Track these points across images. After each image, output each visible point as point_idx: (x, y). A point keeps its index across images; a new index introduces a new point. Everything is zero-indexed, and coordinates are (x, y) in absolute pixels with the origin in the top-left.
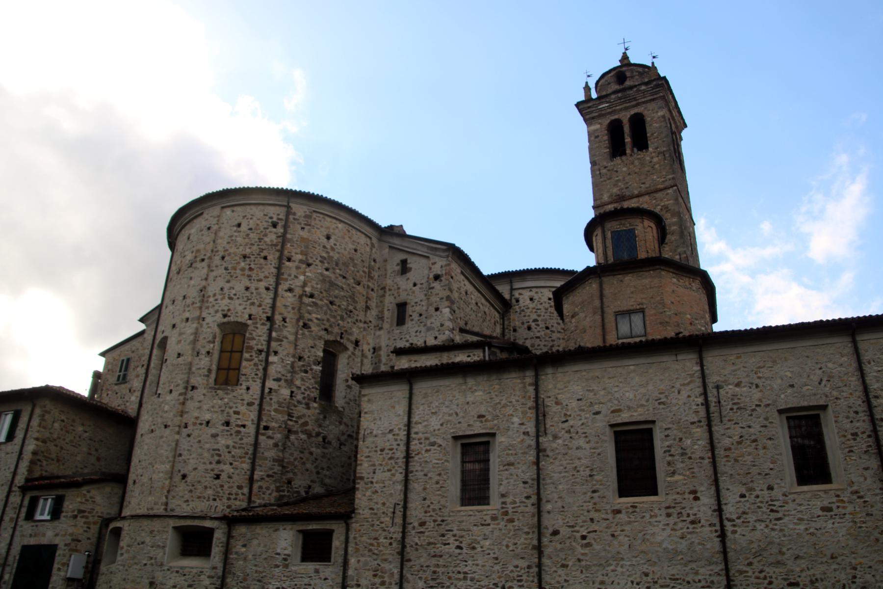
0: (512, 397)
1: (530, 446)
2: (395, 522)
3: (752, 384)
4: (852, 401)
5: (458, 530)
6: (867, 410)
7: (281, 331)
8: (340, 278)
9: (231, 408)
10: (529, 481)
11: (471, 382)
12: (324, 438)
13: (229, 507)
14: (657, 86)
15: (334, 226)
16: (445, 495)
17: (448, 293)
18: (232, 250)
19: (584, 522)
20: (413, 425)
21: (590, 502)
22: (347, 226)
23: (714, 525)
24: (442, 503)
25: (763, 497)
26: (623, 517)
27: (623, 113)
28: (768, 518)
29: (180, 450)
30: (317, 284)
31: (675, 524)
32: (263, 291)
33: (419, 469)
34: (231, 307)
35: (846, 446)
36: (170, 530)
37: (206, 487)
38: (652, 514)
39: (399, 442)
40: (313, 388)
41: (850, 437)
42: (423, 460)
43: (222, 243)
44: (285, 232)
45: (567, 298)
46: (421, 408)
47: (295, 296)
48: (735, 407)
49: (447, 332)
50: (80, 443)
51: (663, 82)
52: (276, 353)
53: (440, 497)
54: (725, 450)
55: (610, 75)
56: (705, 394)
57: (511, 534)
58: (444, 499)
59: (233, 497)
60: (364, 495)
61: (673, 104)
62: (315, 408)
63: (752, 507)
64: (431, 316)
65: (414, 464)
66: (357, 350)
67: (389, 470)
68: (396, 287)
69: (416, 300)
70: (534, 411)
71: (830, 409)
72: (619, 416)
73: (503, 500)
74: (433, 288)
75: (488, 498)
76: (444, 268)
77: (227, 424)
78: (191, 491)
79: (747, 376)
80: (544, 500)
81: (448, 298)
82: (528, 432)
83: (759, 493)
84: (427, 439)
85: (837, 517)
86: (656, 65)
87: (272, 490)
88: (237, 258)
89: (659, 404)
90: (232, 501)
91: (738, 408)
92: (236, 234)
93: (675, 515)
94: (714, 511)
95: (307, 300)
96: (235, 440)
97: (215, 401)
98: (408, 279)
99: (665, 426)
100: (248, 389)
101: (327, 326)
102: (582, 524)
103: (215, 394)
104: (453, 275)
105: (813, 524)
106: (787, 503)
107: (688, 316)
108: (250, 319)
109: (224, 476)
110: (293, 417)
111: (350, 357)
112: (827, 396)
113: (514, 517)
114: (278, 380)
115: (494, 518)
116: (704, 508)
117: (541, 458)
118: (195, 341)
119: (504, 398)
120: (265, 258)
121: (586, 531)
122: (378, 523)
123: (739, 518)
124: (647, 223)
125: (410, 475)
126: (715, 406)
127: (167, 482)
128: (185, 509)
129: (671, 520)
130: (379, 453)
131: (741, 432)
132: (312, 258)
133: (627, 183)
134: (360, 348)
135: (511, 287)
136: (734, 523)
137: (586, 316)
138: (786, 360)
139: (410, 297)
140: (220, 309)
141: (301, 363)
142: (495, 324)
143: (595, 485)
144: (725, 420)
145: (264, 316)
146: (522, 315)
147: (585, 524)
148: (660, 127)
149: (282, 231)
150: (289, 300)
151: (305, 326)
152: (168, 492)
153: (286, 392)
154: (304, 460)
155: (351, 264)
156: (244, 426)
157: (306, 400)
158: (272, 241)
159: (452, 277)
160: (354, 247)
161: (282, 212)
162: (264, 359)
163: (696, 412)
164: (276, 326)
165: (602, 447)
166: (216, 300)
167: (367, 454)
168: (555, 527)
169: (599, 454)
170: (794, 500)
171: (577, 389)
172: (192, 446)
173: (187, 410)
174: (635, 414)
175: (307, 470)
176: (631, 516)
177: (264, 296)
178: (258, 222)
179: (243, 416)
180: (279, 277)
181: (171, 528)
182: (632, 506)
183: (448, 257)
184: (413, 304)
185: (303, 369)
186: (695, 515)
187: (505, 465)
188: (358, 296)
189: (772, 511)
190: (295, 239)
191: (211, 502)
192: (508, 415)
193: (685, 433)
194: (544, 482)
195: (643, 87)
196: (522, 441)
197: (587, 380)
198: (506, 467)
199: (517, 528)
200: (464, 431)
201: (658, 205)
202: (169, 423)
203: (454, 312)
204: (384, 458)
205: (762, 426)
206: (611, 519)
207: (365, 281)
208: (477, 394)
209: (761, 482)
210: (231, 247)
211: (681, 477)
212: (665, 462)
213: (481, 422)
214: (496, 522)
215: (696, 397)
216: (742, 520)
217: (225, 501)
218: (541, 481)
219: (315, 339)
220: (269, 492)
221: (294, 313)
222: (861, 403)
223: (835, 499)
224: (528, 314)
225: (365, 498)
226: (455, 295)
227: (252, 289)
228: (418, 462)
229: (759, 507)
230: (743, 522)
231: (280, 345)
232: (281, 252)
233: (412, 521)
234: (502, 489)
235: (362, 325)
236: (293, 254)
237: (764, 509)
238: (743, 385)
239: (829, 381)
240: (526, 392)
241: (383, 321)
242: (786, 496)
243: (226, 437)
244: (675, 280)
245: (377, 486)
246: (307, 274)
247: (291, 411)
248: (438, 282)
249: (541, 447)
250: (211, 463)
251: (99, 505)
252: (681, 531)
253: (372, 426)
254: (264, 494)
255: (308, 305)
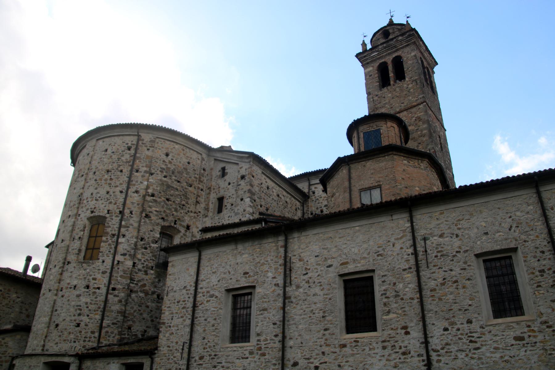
0: (268, 257)
1: (279, 295)
2: (183, 356)
3: (453, 234)
4: (538, 242)
5: (226, 362)
6: (552, 249)
7: (129, 220)
8: (175, 182)
9: (91, 276)
10: (278, 323)
11: (240, 247)
12: (158, 296)
13: (84, 347)
14: (410, 36)
15: (172, 147)
16: (218, 335)
17: (251, 188)
18: (100, 168)
19: (317, 355)
20: (199, 282)
21: (322, 338)
22: (182, 146)
23: (422, 356)
24: (216, 341)
25: (463, 330)
26: (347, 350)
27: (388, 57)
28: (468, 348)
29: (56, 307)
30: (157, 187)
31: (389, 355)
32: (118, 193)
33: (202, 315)
34: (97, 206)
35: (534, 282)
36: (41, 365)
37: (70, 333)
38: (371, 347)
39: (190, 295)
40: (151, 260)
41: (538, 273)
42: (204, 308)
43: (95, 163)
44: (136, 153)
45: (329, 183)
46: (206, 269)
47: (140, 196)
48: (439, 254)
49: (247, 215)
50: (14, 306)
51: (414, 32)
52: (124, 236)
53: (214, 337)
54: (431, 291)
55: (379, 33)
56: (414, 245)
57: (263, 365)
58: (217, 338)
59: (87, 339)
60: (165, 336)
61: (424, 48)
62: (152, 274)
63: (454, 339)
64: (238, 205)
65: (199, 311)
66: (188, 232)
67: (182, 317)
68: (217, 186)
69: (230, 195)
70: (283, 267)
71: (519, 251)
72: (347, 267)
73: (258, 338)
74: (240, 185)
75: (249, 337)
76: (247, 170)
77: (88, 287)
78: (60, 336)
79: (449, 228)
80: (288, 338)
81: (250, 191)
82: (278, 284)
83: (460, 326)
84: (208, 292)
85: (529, 345)
86: (409, 22)
87: (116, 334)
88: (103, 172)
89: (378, 256)
90: (87, 342)
91: (441, 256)
92: (104, 156)
93: (390, 348)
94: (422, 343)
95: (149, 198)
96: (91, 299)
97: (81, 272)
98: (225, 180)
99: (382, 274)
100: (103, 262)
101: (164, 215)
102: (315, 357)
103: (81, 266)
104: (254, 174)
105: (507, 352)
106: (484, 334)
107: (417, 189)
108: (108, 213)
109: (82, 324)
110: (134, 281)
111: (182, 237)
112: (516, 240)
113: (266, 352)
114: (124, 255)
115: (251, 353)
116: (414, 341)
117: (287, 303)
118: (73, 230)
119: (263, 258)
120: (121, 171)
121: (319, 363)
122: (172, 357)
123: (442, 349)
124: (389, 124)
125: (196, 320)
126: (423, 255)
127: (46, 330)
128: (53, 348)
129: (386, 352)
130: (176, 304)
131: (445, 275)
132: (154, 169)
133: (392, 104)
134: (191, 231)
135: (309, 183)
136: (439, 353)
137: (340, 195)
138: (481, 212)
139: (226, 193)
140: (90, 208)
141: (143, 242)
142: (296, 210)
143: (326, 324)
144: (431, 266)
145: (118, 211)
146: (317, 202)
147: (318, 356)
148: (413, 63)
149: (134, 152)
150: (136, 198)
151: (147, 216)
152: (46, 337)
153: (129, 263)
154: (142, 311)
155: (185, 173)
156: (99, 288)
157: (145, 269)
158: (126, 159)
159: (253, 177)
160: (187, 161)
161: (135, 139)
162: (115, 240)
163: (407, 261)
164: (125, 217)
165: (332, 293)
166: (88, 202)
167: (168, 305)
168: (295, 359)
169: (330, 299)
170: (490, 332)
171: (315, 248)
172: (63, 304)
173: (63, 279)
174: (359, 265)
175: (144, 319)
176: (354, 349)
177: (118, 197)
178: (119, 147)
179: (99, 281)
180: (129, 183)
181: (42, 363)
182: (355, 341)
183: (250, 162)
184: (228, 197)
185: (144, 246)
186: (406, 347)
187: (261, 311)
188: (190, 194)
189: (471, 341)
190: (142, 157)
191: (73, 344)
192: (265, 271)
193: (398, 278)
194: (288, 323)
195: (400, 38)
196: (274, 291)
197: (323, 240)
198: (261, 312)
199: (267, 360)
200: (233, 285)
201: (414, 117)
202: (52, 288)
203: (255, 201)
204: (179, 308)
205: (462, 269)
206: (338, 352)
207: (196, 184)
208: (244, 256)
209: (462, 317)
210: (100, 166)
211: (395, 315)
212: (382, 303)
213: (246, 277)
214: (253, 356)
215: (407, 248)
216: (445, 350)
217: (82, 342)
218: (286, 323)
219: (153, 225)
220: (114, 335)
221: (139, 208)
222: (546, 244)
223: (526, 329)
224: (321, 201)
225: (165, 339)
226: (256, 189)
227: (111, 193)
228: (201, 310)
229: (460, 339)
230: (446, 352)
231: (127, 230)
232: (132, 166)
233: (194, 356)
234: (258, 330)
235: (192, 214)
236: (140, 167)
237: (464, 340)
238: (445, 235)
239: (518, 227)
240: (278, 253)
241: (208, 211)
242: (483, 328)
243: (86, 296)
244: (405, 162)
245: (173, 329)
246: (150, 180)
247: (133, 277)
248: (243, 180)
249: (287, 296)
250: (74, 315)
251: (11, 348)
252: (395, 361)
253: (173, 284)
254: (109, 337)
255: (150, 202)
